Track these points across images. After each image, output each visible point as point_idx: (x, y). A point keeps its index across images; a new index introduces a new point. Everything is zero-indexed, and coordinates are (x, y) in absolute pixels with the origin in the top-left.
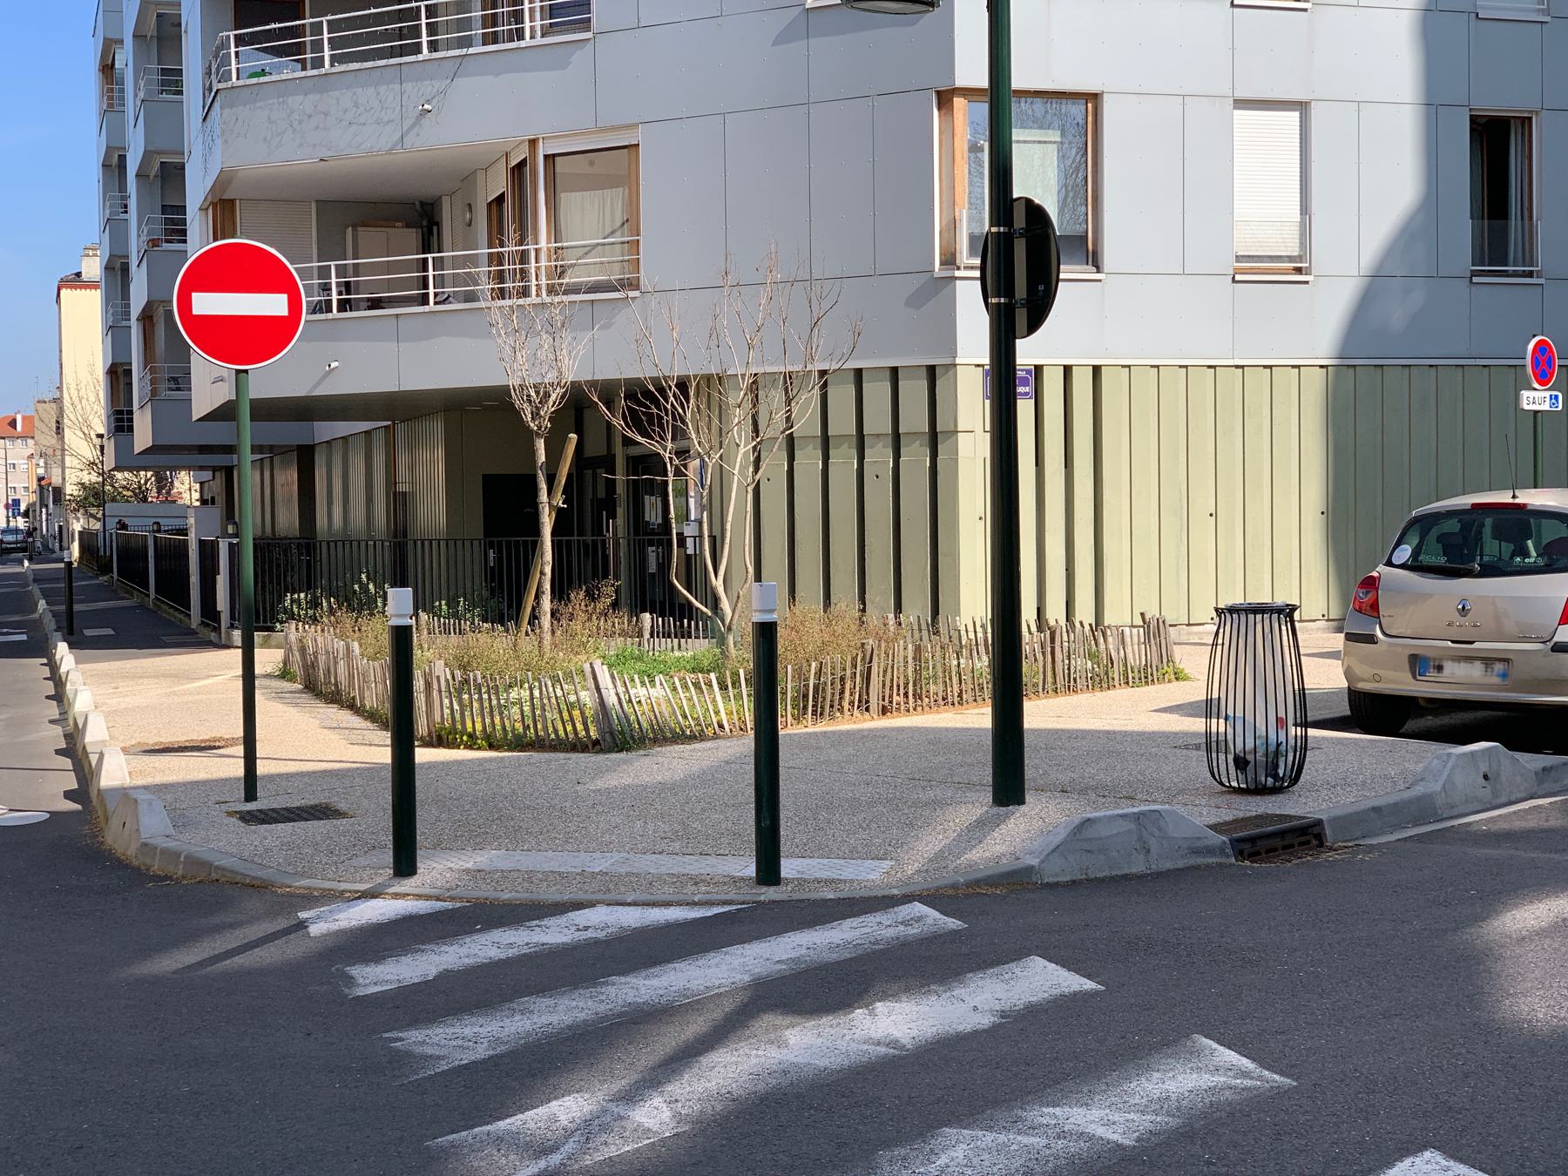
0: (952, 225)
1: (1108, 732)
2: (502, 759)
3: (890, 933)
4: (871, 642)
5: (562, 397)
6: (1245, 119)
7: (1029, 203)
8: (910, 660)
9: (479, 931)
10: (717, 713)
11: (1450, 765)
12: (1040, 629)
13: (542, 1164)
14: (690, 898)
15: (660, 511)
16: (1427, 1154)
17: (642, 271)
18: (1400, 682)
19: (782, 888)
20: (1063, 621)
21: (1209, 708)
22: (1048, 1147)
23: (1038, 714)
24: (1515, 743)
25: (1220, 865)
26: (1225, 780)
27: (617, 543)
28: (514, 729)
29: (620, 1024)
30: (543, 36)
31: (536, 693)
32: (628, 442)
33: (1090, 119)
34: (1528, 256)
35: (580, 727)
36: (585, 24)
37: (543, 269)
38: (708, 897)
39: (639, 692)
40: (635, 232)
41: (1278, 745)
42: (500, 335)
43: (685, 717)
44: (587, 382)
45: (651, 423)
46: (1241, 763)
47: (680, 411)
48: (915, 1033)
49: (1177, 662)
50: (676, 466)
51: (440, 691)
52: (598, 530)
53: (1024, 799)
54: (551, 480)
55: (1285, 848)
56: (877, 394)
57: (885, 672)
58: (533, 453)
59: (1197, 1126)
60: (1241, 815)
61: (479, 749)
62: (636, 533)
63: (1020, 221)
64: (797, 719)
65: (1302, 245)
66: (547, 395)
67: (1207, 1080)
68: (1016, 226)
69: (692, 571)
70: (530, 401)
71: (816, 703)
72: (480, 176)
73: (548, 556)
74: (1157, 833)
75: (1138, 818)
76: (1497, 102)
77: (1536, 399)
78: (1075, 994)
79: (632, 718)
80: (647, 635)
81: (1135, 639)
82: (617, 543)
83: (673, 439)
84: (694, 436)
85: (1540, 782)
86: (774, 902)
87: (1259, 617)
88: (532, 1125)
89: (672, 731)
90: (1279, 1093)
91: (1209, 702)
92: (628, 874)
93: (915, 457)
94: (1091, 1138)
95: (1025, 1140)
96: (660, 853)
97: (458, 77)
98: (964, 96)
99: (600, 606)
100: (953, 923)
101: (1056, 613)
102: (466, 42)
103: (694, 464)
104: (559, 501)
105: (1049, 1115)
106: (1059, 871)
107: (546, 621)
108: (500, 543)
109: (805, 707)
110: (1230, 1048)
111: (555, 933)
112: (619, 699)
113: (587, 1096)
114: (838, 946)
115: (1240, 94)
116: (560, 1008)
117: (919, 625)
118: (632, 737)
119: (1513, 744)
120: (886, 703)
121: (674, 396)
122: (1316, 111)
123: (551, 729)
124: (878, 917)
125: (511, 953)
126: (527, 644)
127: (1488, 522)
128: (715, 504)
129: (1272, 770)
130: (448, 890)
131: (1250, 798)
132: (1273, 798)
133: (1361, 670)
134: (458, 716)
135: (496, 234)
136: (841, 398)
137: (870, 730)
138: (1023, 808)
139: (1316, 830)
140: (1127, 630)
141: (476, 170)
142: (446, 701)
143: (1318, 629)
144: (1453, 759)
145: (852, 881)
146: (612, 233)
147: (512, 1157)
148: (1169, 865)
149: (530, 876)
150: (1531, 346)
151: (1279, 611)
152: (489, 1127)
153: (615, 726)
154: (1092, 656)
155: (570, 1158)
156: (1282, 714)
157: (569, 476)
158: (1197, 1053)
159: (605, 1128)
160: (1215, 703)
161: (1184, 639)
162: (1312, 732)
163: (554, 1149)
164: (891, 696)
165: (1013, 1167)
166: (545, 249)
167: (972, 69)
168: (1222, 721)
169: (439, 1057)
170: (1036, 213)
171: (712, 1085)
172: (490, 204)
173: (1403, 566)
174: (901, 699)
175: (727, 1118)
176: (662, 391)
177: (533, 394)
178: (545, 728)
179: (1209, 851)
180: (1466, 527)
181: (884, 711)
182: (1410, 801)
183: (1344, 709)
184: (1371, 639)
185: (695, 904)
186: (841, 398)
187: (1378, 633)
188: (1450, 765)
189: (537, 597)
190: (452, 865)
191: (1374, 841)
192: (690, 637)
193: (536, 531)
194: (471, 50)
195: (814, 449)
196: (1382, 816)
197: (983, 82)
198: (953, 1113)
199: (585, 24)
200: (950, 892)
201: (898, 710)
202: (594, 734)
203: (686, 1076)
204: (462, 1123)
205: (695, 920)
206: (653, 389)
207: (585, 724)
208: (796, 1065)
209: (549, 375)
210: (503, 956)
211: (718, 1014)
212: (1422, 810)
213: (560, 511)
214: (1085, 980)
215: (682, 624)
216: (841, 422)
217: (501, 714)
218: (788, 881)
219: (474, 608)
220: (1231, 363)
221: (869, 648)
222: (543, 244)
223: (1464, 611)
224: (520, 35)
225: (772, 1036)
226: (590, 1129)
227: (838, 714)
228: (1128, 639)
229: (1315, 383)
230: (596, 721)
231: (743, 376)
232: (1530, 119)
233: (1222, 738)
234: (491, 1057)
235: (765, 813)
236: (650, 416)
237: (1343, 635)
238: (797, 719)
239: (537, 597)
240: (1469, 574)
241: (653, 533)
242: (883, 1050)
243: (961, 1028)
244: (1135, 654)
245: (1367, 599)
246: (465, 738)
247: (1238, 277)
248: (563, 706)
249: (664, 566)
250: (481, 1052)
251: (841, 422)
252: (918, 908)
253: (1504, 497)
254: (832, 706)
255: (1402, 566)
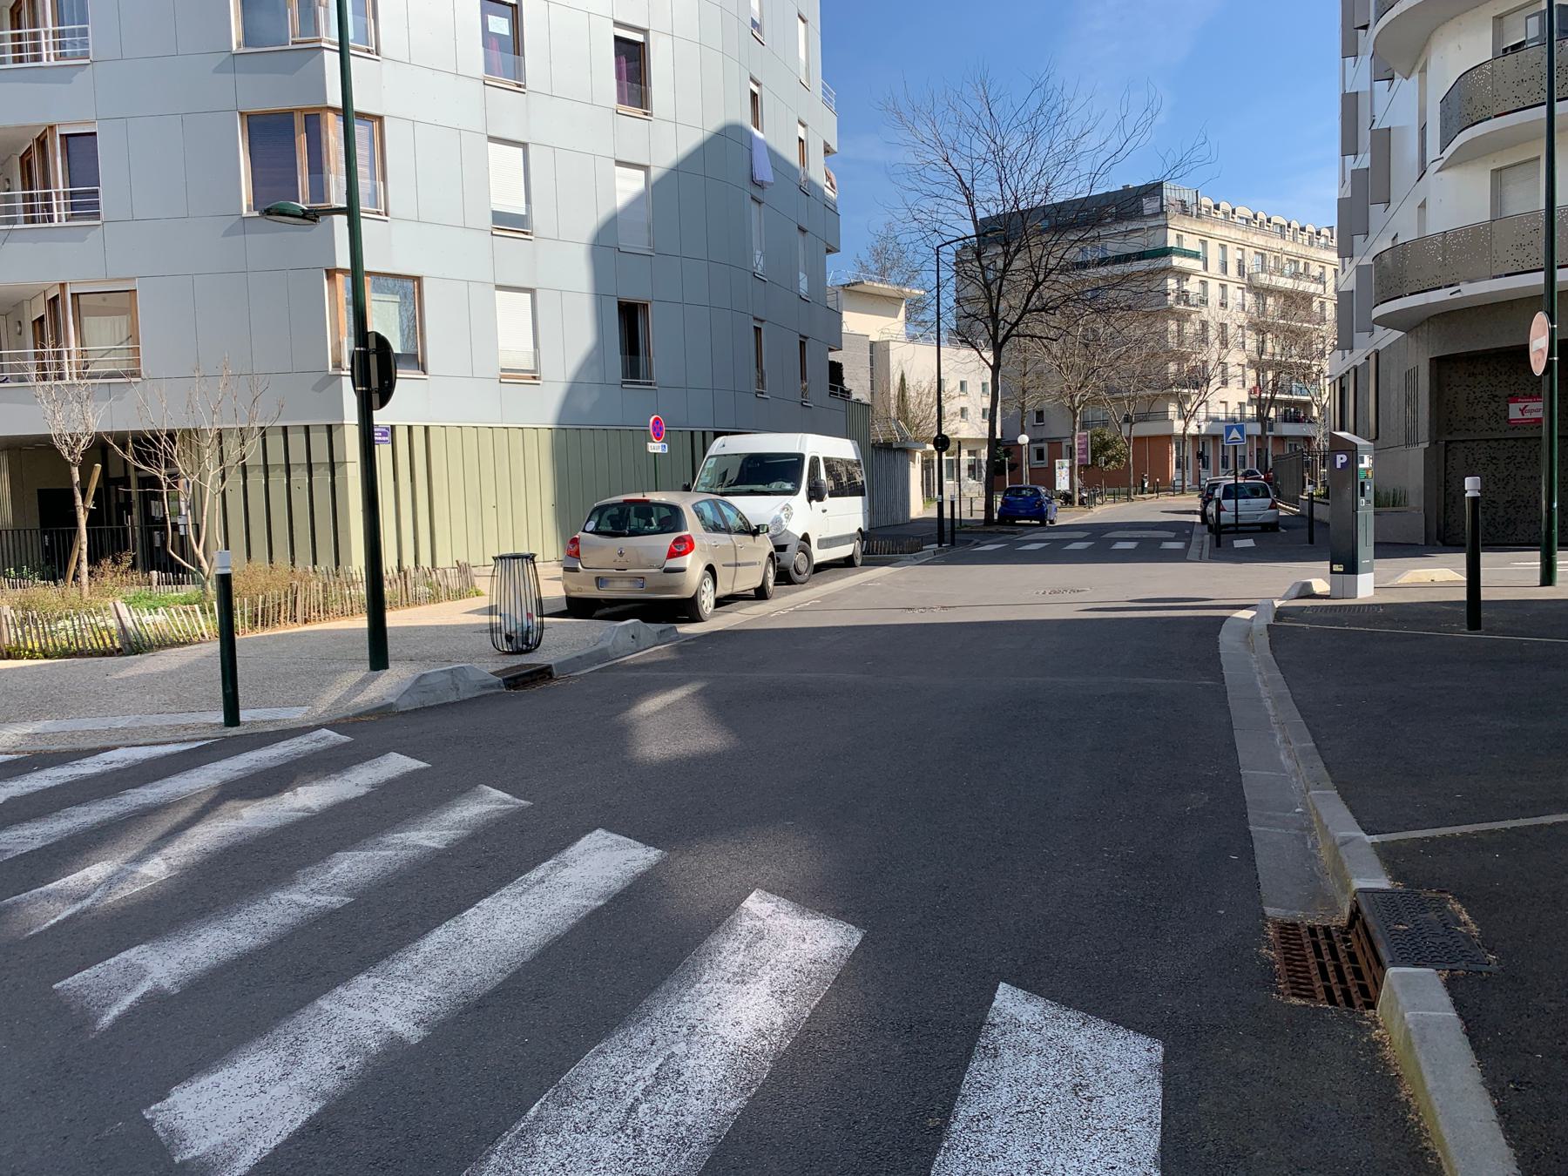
0: (338, 346)
1: (437, 626)
2: (55, 663)
3: (308, 747)
4: (296, 582)
5: (90, 441)
6: (499, 293)
7: (378, 336)
8: (321, 591)
9: (37, 770)
10: (200, 628)
11: (615, 632)
12: (399, 571)
13: (78, 906)
14: (181, 739)
15: (161, 510)
16: (598, 831)
17: (142, 365)
18: (592, 592)
19: (241, 727)
20: (412, 566)
21: (491, 611)
22: (396, 855)
23: (393, 619)
24: (647, 619)
25: (497, 693)
26: (501, 648)
27: (133, 530)
28: (61, 645)
29: (135, 817)
30: (67, 221)
31: (77, 622)
32: (137, 469)
33: (416, 290)
34: (649, 375)
35: (108, 641)
36: (97, 216)
37: (74, 364)
38: (194, 736)
39: (147, 618)
40: (136, 342)
41: (528, 627)
42: (43, 403)
43: (179, 631)
44: (105, 433)
45: (150, 457)
46: (509, 638)
47: (170, 450)
48: (320, 802)
49: (477, 585)
50: (169, 483)
51: (7, 625)
52: (120, 521)
53: (387, 664)
54: (84, 493)
55: (532, 681)
56: (297, 440)
57: (305, 599)
58: (70, 476)
59: (479, 833)
60: (509, 665)
61: (38, 658)
62: (147, 523)
63: (372, 344)
64: (251, 629)
65: (536, 365)
66: (79, 440)
67: (486, 808)
68: (371, 347)
69: (183, 545)
70: (67, 444)
71: (261, 618)
72: (26, 305)
73: (85, 538)
74: (463, 679)
75: (451, 671)
76: (631, 296)
77: (655, 447)
78: (415, 770)
79: (144, 634)
80: (155, 584)
81: (453, 575)
82: (133, 530)
83: (166, 467)
84: (179, 465)
85: (659, 637)
86: (236, 736)
87: (516, 561)
88: (72, 884)
89: (171, 640)
90: (523, 810)
91: (491, 608)
92: (141, 727)
93: (322, 477)
94: (421, 847)
95: (384, 853)
96: (162, 713)
97: (9, 242)
98: (342, 273)
99: (122, 568)
100: (345, 739)
101: (408, 562)
102: (14, 221)
103: (182, 482)
104: (90, 505)
105: (396, 838)
106: (407, 704)
107: (85, 578)
108: (51, 532)
109: (256, 622)
110: (498, 789)
111: (89, 767)
112: (134, 623)
113: (110, 862)
114: (275, 758)
115: (499, 282)
116: (92, 812)
117: (328, 572)
118: (144, 645)
119: (646, 620)
120: (307, 616)
121: (165, 441)
122: (539, 293)
123: (88, 644)
124: (296, 740)
125: (58, 782)
126: (72, 592)
127: (632, 509)
128: (196, 506)
129: (526, 639)
130: (14, 747)
131: (514, 656)
132: (526, 655)
133: (572, 586)
134: (21, 640)
135: (40, 340)
136: (275, 443)
137: (297, 633)
138: (388, 671)
139: (549, 670)
140: (448, 571)
141: (23, 301)
142: (12, 631)
143: (553, 565)
144: (616, 630)
145: (285, 720)
146: (121, 343)
147: (58, 904)
148: (470, 696)
149: (72, 735)
150: (652, 420)
151: (527, 557)
152: (41, 889)
153: (132, 640)
154: (430, 585)
155: (97, 900)
156: (530, 611)
157: (97, 490)
158: (481, 794)
159: (121, 880)
160: (494, 608)
161: (482, 573)
162: (546, 619)
163: (86, 897)
164: (309, 613)
165: (376, 869)
166: (74, 351)
167: (343, 261)
168: (498, 617)
169: (6, 851)
170: (382, 342)
171: (194, 846)
172: (34, 322)
173: (591, 532)
174: (316, 614)
175: (202, 864)
176: (157, 439)
177: (69, 439)
178: (84, 643)
179: (492, 686)
180: (622, 512)
181: (306, 621)
182: (595, 651)
183: (565, 607)
184: (576, 570)
185: (184, 741)
186: (275, 443)
187: (580, 567)
188: (615, 632)
189: (78, 564)
190: (16, 732)
191: (578, 674)
192: (183, 584)
193: (75, 523)
194: (16, 227)
195: (325, 470)
196: (581, 661)
197: (348, 266)
198: (341, 844)
199: (97, 216)
200: (345, 721)
201: (314, 620)
202: (117, 645)
203: (177, 843)
204: (23, 888)
205: (184, 752)
206: (150, 437)
207: (111, 639)
208: (247, 828)
209: (80, 428)
210: (53, 785)
211: (199, 805)
212: (602, 656)
213: (91, 511)
214: (408, 759)
215: (178, 577)
216: (276, 457)
217: (52, 636)
218: (245, 723)
219: (35, 572)
220: (500, 425)
221: (294, 586)
222: (73, 346)
223: (621, 554)
224: (51, 219)
225: (232, 814)
226: (110, 882)
227: (277, 625)
228: (449, 575)
229: (546, 437)
230: (119, 637)
231: (210, 430)
232: (647, 305)
233: (498, 626)
234: (43, 847)
235: (229, 685)
236: (149, 454)
237: (562, 569)
238: (251, 629)
239: (78, 564)
240: (624, 535)
241: (157, 522)
242: (300, 814)
243: (348, 797)
244: (454, 582)
245: (574, 549)
246: (27, 653)
247: (502, 380)
248: (95, 630)
249: (164, 543)
250: (37, 844)
251: (276, 457)
252: (325, 732)
253: (639, 496)
254: (273, 620)
255: (591, 532)
